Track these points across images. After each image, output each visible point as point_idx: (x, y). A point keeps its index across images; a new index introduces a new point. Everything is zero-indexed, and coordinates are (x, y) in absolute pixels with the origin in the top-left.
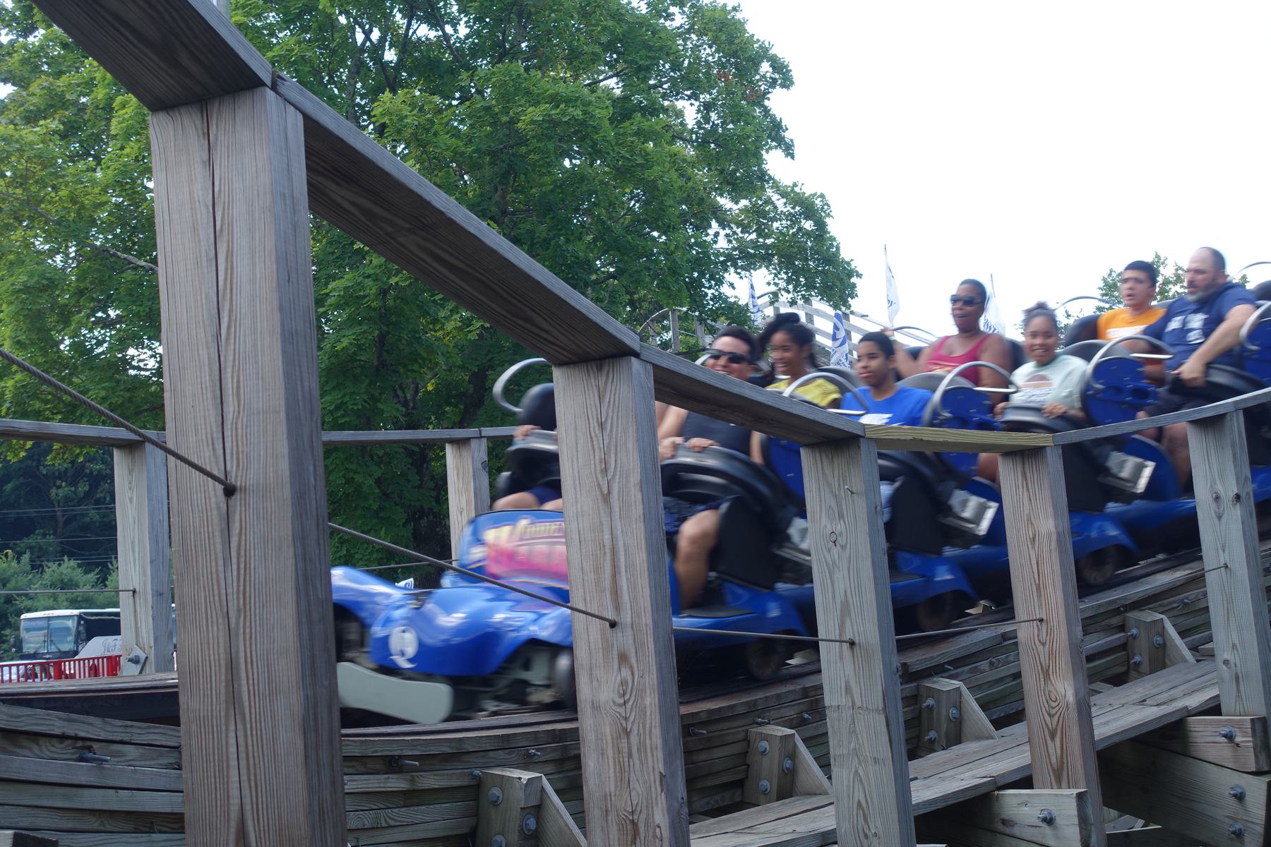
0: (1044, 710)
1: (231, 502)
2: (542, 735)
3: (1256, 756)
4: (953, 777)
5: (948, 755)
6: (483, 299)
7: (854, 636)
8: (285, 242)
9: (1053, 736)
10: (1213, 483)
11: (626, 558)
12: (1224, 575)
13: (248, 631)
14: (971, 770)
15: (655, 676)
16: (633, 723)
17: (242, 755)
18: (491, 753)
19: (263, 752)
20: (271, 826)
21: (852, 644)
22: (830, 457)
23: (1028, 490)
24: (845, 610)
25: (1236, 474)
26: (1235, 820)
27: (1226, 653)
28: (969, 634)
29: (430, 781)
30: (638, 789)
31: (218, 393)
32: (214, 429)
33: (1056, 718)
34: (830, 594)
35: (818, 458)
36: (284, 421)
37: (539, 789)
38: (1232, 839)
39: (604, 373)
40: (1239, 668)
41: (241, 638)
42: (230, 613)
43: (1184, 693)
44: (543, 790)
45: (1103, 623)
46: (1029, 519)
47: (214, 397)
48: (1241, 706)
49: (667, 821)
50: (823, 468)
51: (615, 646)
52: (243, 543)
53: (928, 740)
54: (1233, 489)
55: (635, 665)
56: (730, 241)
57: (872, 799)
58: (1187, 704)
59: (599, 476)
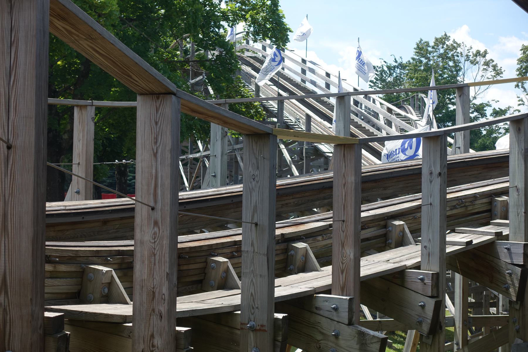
0: (340, 261)
1: (10, 152)
2: (113, 252)
4: (297, 287)
5: (297, 277)
6: (112, 67)
8: (40, 50)
9: (342, 273)
10: (430, 167)
11: (161, 181)
12: (430, 208)
13: (12, 203)
14: (306, 284)
15: (168, 232)
16: (157, 251)
17: (7, 251)
18: (90, 258)
19: (15, 249)
20: (16, 279)
21: (256, 224)
23: (345, 162)
25: (441, 163)
26: (420, 316)
28: (306, 225)
29: (62, 268)
30: (157, 278)
31: (8, 107)
32: (5, 122)
33: (345, 265)
35: (251, 139)
36: (34, 122)
37: (111, 275)
38: (417, 325)
39: (160, 100)
40: (430, 250)
41: (10, 205)
42: (6, 195)
43: (406, 259)
44: (112, 276)
45: (377, 223)
46: (344, 176)
47: (6, 109)
48: (429, 268)
49: (168, 292)
50: (252, 146)
51: (153, 218)
52: (13, 168)
54: (438, 170)
55: (161, 227)
56: (227, 5)
57: (257, 293)
59: (153, 145)
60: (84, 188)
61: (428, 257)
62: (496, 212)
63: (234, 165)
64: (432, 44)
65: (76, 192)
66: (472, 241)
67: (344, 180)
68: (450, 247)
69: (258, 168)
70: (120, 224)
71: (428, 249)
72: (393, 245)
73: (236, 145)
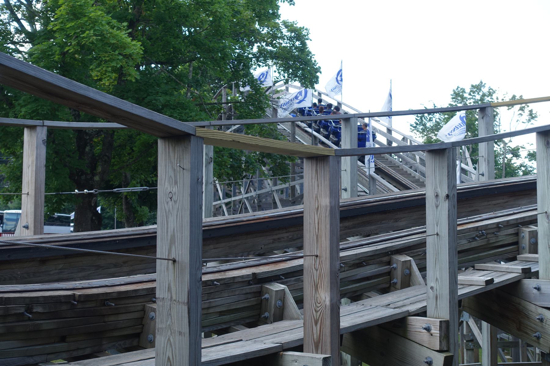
3: (440, 341)
4: (262, 341)
7: (176, 256)
9: (316, 324)
10: (436, 188)
12: (436, 240)
14: (275, 337)
21: (174, 261)
22: (174, 146)
23: (318, 180)
24: (172, 241)
27: (432, 283)
33: (319, 313)
34: (166, 229)
35: (167, 146)
40: (438, 292)
43: (411, 302)
45: (378, 260)
46: (317, 197)
53: (263, 317)
57: (176, 356)
58: (409, 309)
60: (33, 222)
61: (435, 300)
62: (524, 245)
63: (272, 207)
64: (468, 90)
65: (24, 227)
66: (493, 279)
67: (316, 202)
68: (466, 287)
69: (176, 183)
70: (65, 264)
71: (435, 290)
72: (399, 285)
73: (274, 186)
